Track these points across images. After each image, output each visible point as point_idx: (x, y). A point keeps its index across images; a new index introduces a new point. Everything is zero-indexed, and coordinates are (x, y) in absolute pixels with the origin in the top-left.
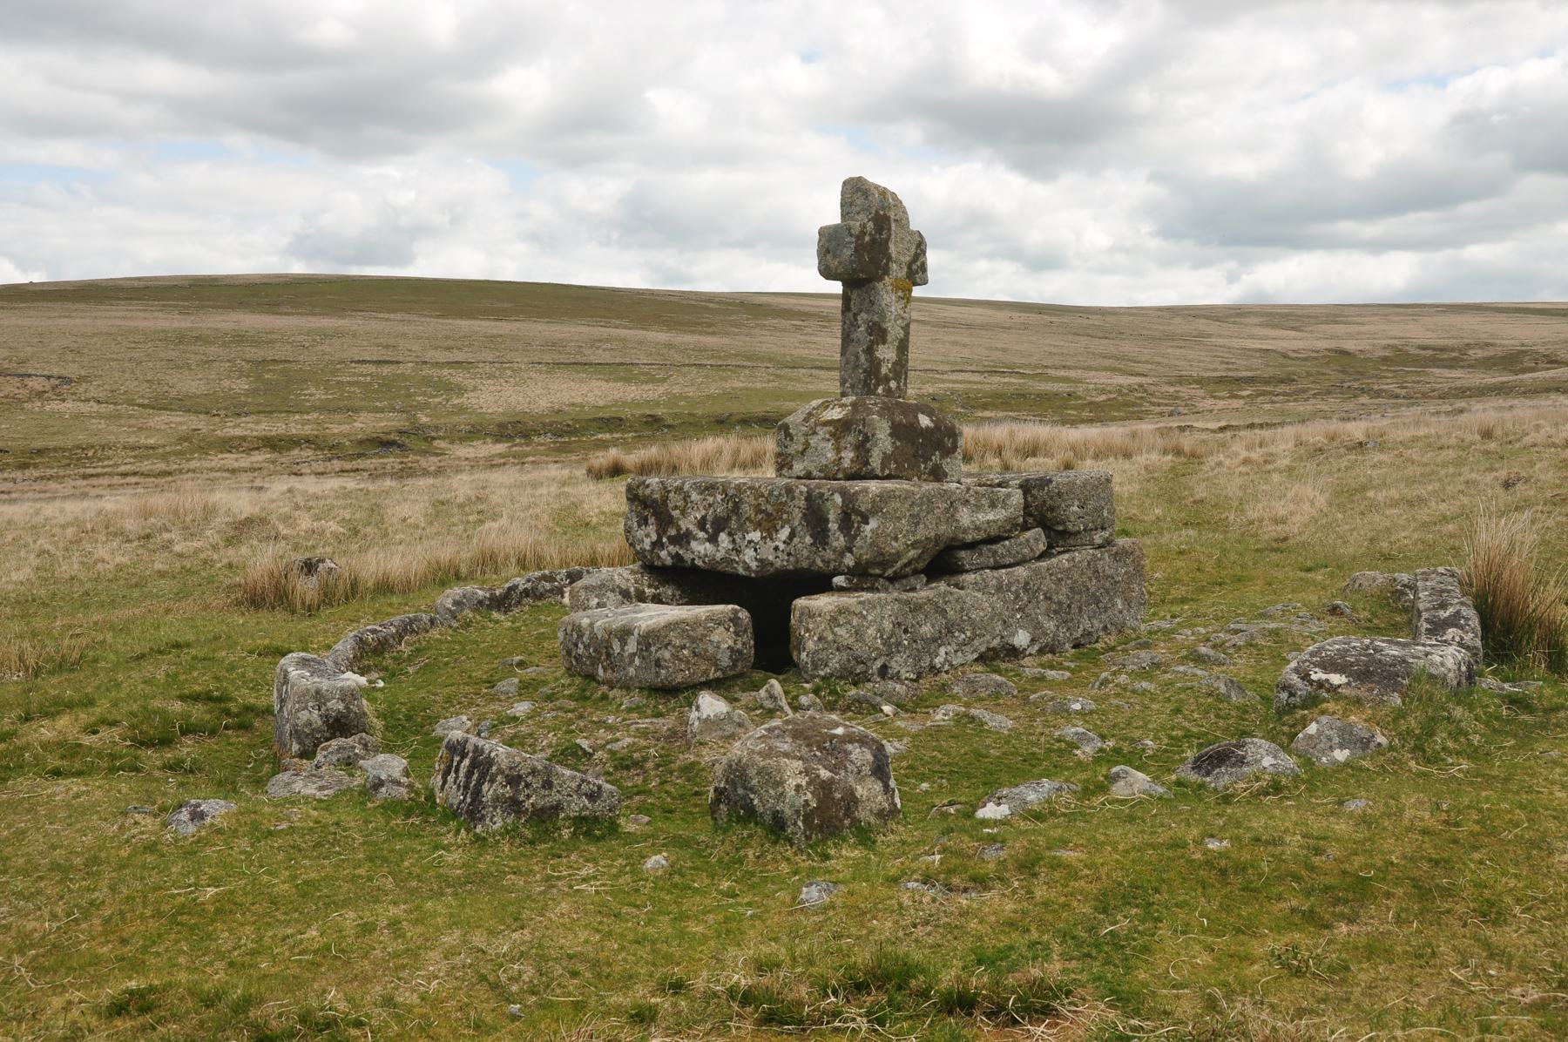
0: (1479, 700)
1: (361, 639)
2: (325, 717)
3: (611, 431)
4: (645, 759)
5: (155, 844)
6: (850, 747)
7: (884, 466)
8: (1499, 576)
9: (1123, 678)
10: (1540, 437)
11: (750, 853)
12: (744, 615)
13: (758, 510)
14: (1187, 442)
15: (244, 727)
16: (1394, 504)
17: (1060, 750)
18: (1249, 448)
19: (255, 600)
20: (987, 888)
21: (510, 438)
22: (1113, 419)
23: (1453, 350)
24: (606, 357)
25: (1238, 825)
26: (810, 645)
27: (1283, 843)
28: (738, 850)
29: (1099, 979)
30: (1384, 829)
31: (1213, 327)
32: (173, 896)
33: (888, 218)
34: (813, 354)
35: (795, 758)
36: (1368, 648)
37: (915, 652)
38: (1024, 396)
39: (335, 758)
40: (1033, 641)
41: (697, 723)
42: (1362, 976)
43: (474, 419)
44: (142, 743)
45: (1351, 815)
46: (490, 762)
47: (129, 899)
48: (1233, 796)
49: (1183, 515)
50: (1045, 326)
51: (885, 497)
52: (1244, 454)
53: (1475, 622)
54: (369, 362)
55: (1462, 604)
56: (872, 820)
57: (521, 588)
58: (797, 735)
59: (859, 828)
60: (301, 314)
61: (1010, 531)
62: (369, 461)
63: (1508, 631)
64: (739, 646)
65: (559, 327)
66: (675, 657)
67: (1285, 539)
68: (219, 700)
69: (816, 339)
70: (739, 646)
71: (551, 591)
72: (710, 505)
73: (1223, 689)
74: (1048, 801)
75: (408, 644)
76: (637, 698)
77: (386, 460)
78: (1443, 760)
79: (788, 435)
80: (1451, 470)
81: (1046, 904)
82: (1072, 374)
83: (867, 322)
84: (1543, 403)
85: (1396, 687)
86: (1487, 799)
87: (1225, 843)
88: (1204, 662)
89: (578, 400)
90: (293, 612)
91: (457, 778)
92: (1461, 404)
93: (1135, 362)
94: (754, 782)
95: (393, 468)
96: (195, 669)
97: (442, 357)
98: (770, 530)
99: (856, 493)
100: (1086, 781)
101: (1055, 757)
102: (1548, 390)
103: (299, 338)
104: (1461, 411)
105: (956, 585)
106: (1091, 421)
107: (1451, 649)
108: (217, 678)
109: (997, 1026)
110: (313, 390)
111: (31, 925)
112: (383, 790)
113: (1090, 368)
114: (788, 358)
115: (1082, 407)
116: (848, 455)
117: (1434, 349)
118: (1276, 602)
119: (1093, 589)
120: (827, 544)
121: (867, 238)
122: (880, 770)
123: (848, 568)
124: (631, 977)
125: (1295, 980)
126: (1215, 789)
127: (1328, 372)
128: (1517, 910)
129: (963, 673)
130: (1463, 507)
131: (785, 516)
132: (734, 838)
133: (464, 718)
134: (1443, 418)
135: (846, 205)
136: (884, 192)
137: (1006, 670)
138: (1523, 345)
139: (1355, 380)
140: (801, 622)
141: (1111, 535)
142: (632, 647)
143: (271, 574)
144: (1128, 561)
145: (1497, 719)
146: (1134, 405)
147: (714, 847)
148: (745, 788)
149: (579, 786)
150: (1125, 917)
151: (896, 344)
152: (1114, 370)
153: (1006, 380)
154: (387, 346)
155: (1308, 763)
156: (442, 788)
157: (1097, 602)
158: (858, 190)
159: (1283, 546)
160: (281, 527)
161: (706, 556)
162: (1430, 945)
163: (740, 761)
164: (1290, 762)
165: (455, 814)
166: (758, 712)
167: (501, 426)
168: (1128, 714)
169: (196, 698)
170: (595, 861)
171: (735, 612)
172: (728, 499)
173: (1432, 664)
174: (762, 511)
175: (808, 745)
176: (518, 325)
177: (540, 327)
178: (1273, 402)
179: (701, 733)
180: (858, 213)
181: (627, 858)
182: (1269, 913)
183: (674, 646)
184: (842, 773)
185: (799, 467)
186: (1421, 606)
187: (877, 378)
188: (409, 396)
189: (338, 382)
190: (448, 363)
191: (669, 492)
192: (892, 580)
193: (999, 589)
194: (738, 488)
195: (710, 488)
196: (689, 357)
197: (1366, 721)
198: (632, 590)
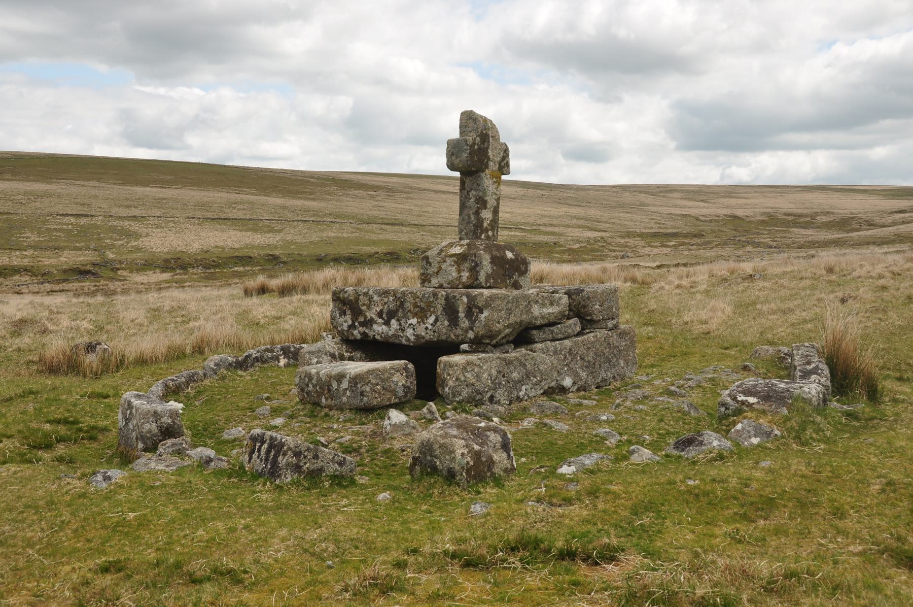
0: (830, 413)
1: (166, 384)
2: (160, 428)
3: (244, 266)
4: (360, 447)
5: (84, 493)
6: (488, 433)
7: (487, 281)
8: (840, 345)
9: (628, 403)
10: (863, 272)
11: (436, 491)
12: (411, 366)
13: (415, 306)
14: (639, 274)
15: (93, 438)
16: (774, 312)
17: (597, 441)
18: (680, 278)
19: (52, 369)
20: (572, 504)
21: (172, 269)
22: (585, 260)
23: (807, 216)
24: (240, 215)
25: (703, 473)
26: (451, 383)
27: (727, 482)
28: (428, 490)
29: (637, 545)
30: (781, 475)
31: (649, 199)
32: (111, 517)
33: (488, 135)
34: (382, 214)
35: (460, 438)
36: (768, 383)
37: (509, 389)
38: (524, 244)
39: (171, 450)
40: (574, 383)
41: (389, 427)
42: (773, 543)
43: (147, 256)
44: (34, 447)
45: (763, 469)
46: (282, 445)
47: (85, 519)
48: (697, 462)
49: (642, 319)
50: (538, 197)
51: (492, 298)
52: (677, 282)
53: (827, 372)
54: (71, 215)
55: (820, 362)
56: (502, 473)
57: (254, 356)
58: (459, 426)
59: (495, 478)
60: (19, 180)
61: (561, 319)
62: (71, 285)
63: (846, 378)
64: (409, 384)
65: (206, 193)
66: (373, 390)
67: (708, 333)
68: (73, 423)
69: (384, 204)
70: (409, 384)
71: (272, 358)
72: (385, 303)
73: (686, 409)
74: (597, 464)
75: (192, 388)
76: (349, 415)
77: (84, 284)
78: (811, 444)
79: (428, 263)
80: (808, 292)
81: (604, 511)
82: (556, 230)
83: (475, 196)
84: (864, 251)
85: (785, 404)
86: (835, 461)
87: (697, 482)
88: (673, 395)
89: (221, 244)
90: (85, 376)
91: (259, 455)
92: (812, 252)
93: (599, 222)
94: (437, 452)
95: (89, 289)
96: (52, 405)
97: (123, 212)
98: (422, 317)
99: (476, 296)
100: (616, 454)
101: (594, 445)
102: (868, 244)
103: (18, 197)
104: (813, 256)
105: (531, 350)
106: (570, 261)
107: (814, 385)
108: (68, 411)
109: (588, 565)
110: (29, 234)
111: (29, 534)
112: (213, 464)
113: (568, 226)
114: (365, 217)
115: (564, 252)
116: (465, 275)
117: (795, 216)
118: (708, 366)
119: (607, 354)
120: (458, 325)
121: (476, 147)
122: (505, 446)
123: (470, 339)
124: (387, 548)
125: (738, 545)
126: (687, 458)
127: (726, 230)
128: (851, 511)
129: (536, 401)
130: (816, 314)
131: (432, 309)
132: (426, 484)
133: (240, 429)
134: (801, 260)
135: (463, 127)
136: (485, 120)
137: (559, 400)
138: (852, 214)
139: (743, 236)
140: (444, 370)
141: (617, 322)
142: (345, 384)
143: (64, 353)
144: (627, 338)
145: (839, 424)
146: (598, 251)
147: (414, 489)
148: (431, 456)
149: (334, 458)
150: (647, 517)
151: (492, 209)
152: (584, 227)
153: (513, 233)
154: (83, 204)
155: (737, 445)
156: (249, 461)
157: (610, 362)
158: (471, 118)
159: (708, 336)
160: (49, 325)
161: (383, 333)
162: (807, 528)
163: (429, 441)
164: (728, 444)
165: (260, 475)
166: (423, 421)
167: (167, 261)
168: (633, 422)
169: (58, 422)
170: (347, 497)
171: (406, 365)
172: (396, 298)
173: (804, 392)
174: (418, 307)
175: (467, 432)
176: (177, 191)
177: (193, 193)
178: (690, 250)
179: (392, 432)
180: (470, 132)
181: (366, 495)
182: (722, 515)
183: (372, 384)
184: (486, 446)
185: (435, 281)
186: (796, 364)
187: (481, 229)
188: (100, 239)
189: (48, 229)
190: (128, 217)
191: (360, 295)
192: (495, 346)
193: (555, 352)
194: (403, 293)
195: (386, 293)
196: (297, 215)
197: (768, 422)
198: (337, 353)
